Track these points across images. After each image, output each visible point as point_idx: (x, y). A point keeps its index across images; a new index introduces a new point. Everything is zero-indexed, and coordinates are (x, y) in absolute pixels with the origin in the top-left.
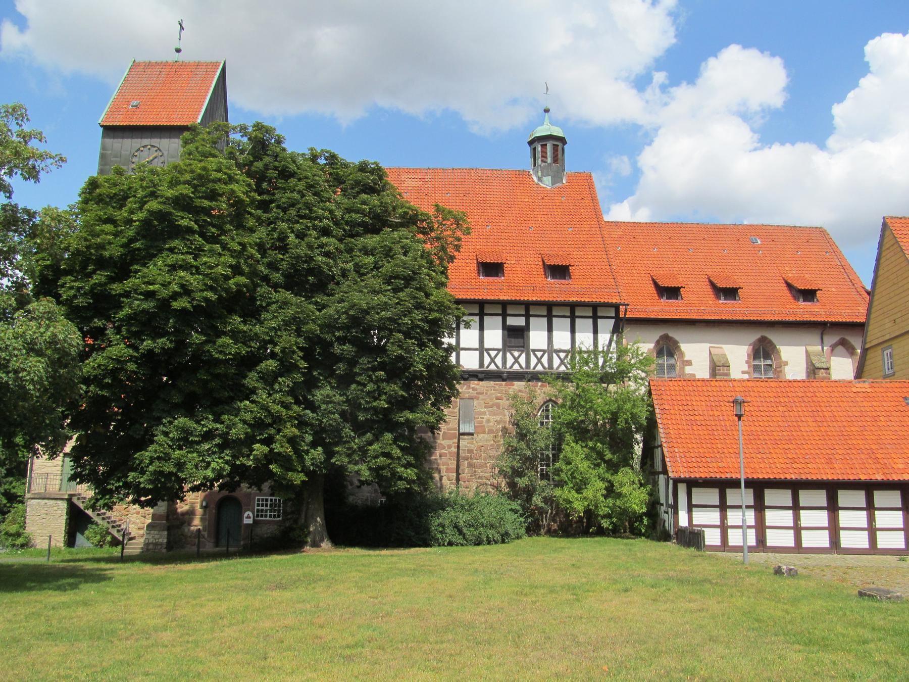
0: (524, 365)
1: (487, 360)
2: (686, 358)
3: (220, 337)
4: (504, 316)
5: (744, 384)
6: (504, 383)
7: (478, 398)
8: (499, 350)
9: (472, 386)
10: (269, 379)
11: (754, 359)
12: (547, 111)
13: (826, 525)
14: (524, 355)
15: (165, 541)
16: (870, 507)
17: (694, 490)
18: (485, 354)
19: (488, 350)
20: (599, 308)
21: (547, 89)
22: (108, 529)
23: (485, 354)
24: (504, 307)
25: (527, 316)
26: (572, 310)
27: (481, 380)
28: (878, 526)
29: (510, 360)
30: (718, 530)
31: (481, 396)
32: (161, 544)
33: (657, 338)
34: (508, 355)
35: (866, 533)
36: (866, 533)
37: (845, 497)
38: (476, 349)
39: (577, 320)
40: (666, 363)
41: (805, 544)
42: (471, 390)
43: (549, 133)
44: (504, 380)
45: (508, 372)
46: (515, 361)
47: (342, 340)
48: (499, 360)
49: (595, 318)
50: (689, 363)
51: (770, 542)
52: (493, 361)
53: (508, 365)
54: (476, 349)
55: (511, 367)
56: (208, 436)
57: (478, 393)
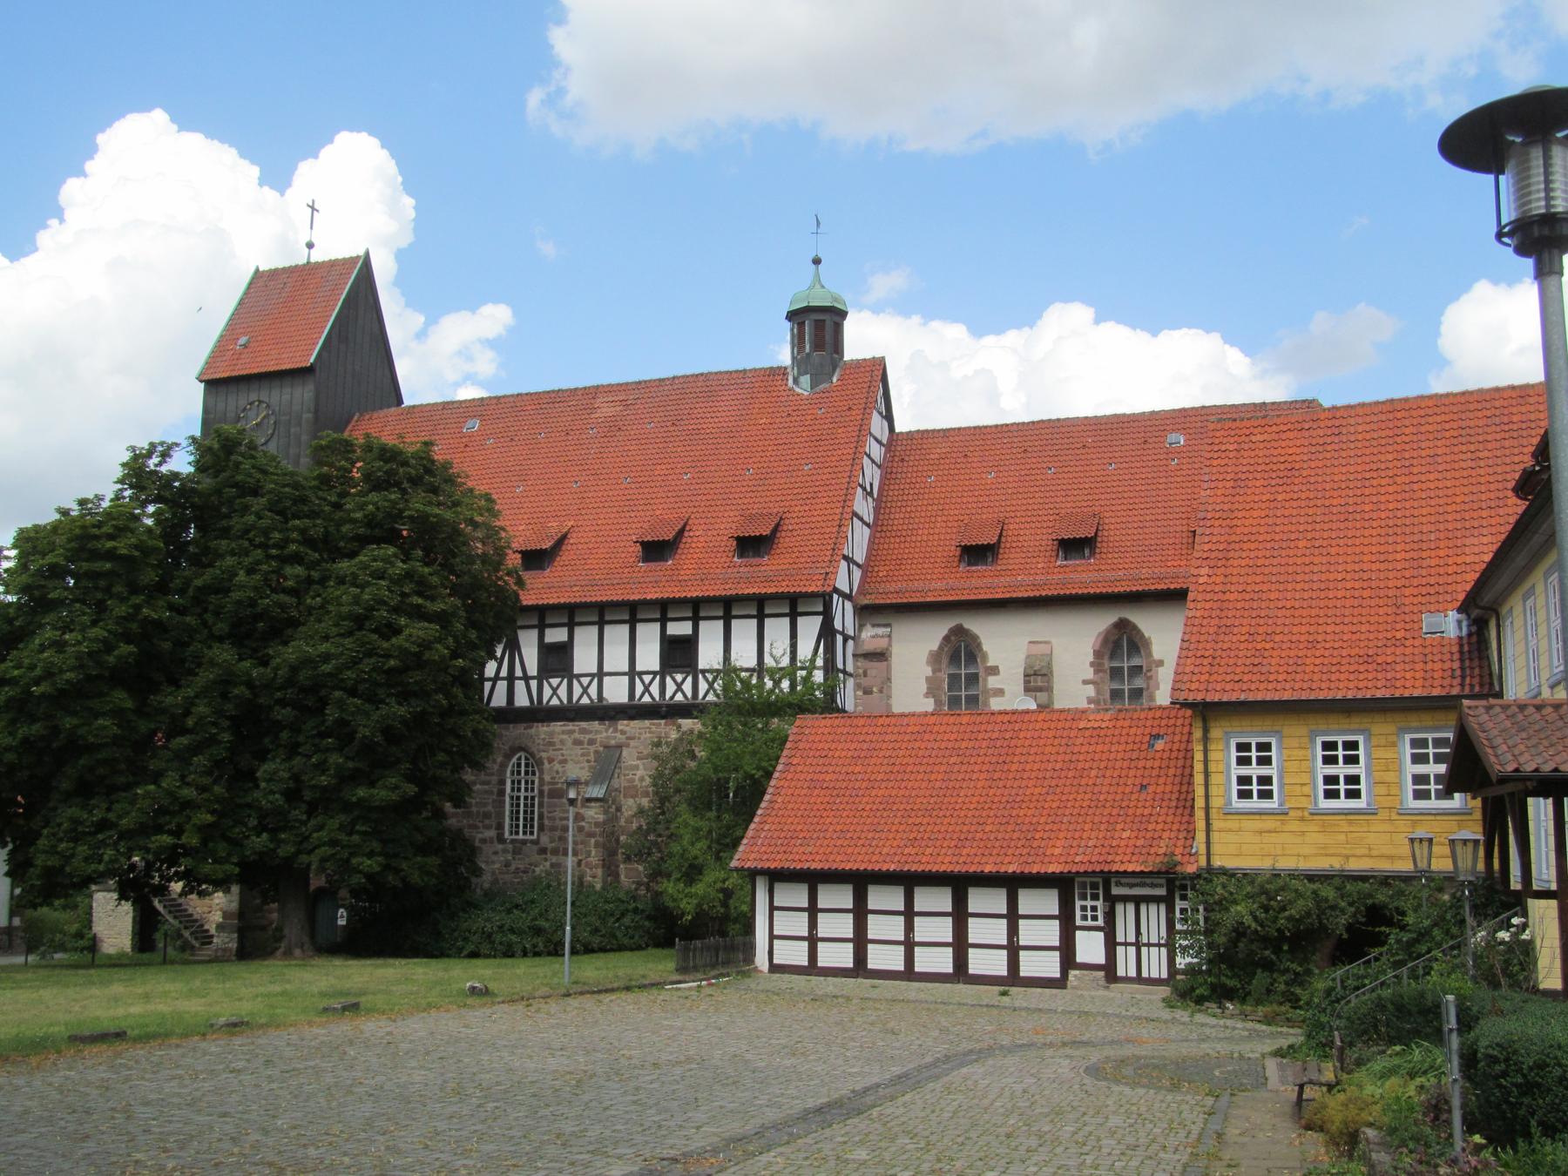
0: (689, 695)
1: (639, 688)
2: (990, 663)
3: (96, 718)
4: (663, 621)
5: (926, 721)
6: (663, 722)
7: (628, 746)
8: (655, 673)
9: (620, 727)
10: (183, 757)
11: (1112, 657)
12: (817, 261)
13: (1057, 944)
14: (690, 679)
15: (235, 945)
16: (1013, 917)
17: (778, 887)
18: (637, 680)
19: (641, 674)
20: (799, 601)
21: (818, 223)
22: (179, 930)
23: (637, 680)
24: (663, 610)
25: (696, 620)
26: (760, 607)
27: (632, 718)
28: (1021, 943)
29: (671, 687)
30: (902, 948)
31: (632, 743)
32: (230, 950)
33: (945, 632)
34: (668, 679)
35: (1005, 952)
36: (1005, 952)
37: (983, 900)
38: (624, 674)
39: (767, 621)
40: (963, 672)
41: (919, 967)
42: (618, 735)
43: (805, 304)
44: (663, 717)
45: (668, 706)
46: (678, 689)
47: (282, 703)
48: (655, 689)
49: (793, 616)
50: (994, 671)
51: (973, 969)
52: (647, 689)
53: (668, 695)
54: (624, 674)
55: (672, 698)
56: (103, 825)
57: (628, 738)
